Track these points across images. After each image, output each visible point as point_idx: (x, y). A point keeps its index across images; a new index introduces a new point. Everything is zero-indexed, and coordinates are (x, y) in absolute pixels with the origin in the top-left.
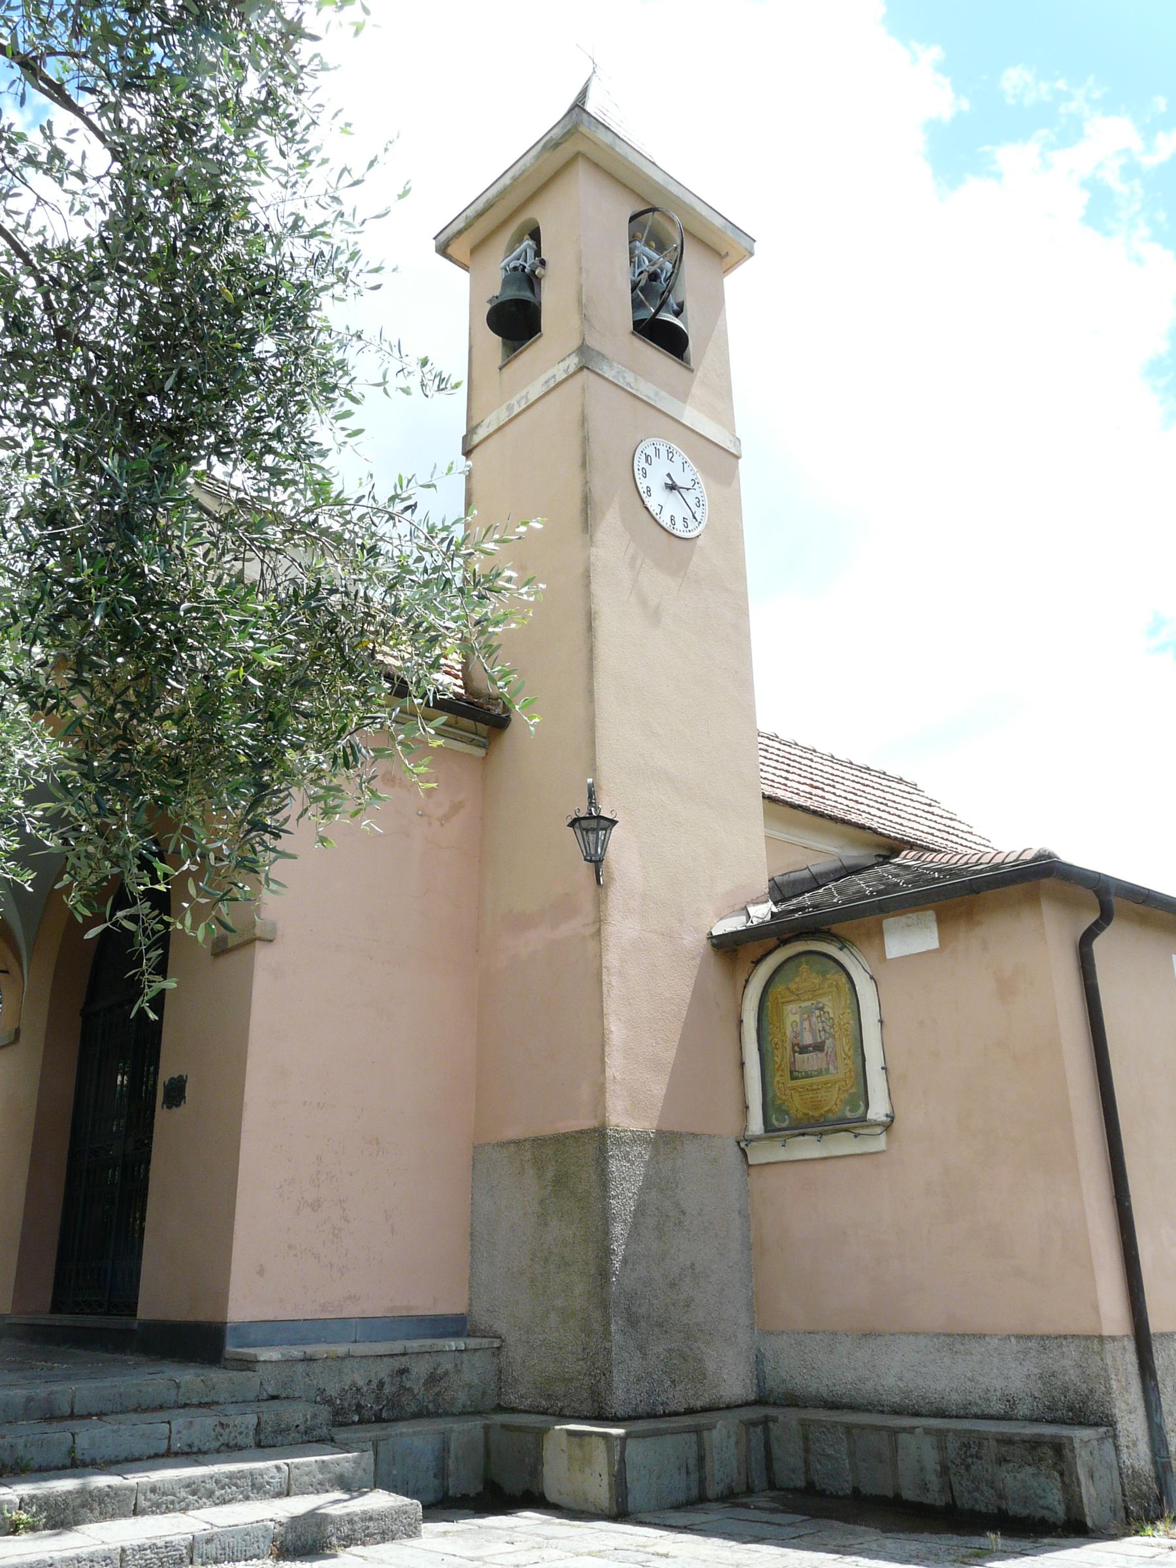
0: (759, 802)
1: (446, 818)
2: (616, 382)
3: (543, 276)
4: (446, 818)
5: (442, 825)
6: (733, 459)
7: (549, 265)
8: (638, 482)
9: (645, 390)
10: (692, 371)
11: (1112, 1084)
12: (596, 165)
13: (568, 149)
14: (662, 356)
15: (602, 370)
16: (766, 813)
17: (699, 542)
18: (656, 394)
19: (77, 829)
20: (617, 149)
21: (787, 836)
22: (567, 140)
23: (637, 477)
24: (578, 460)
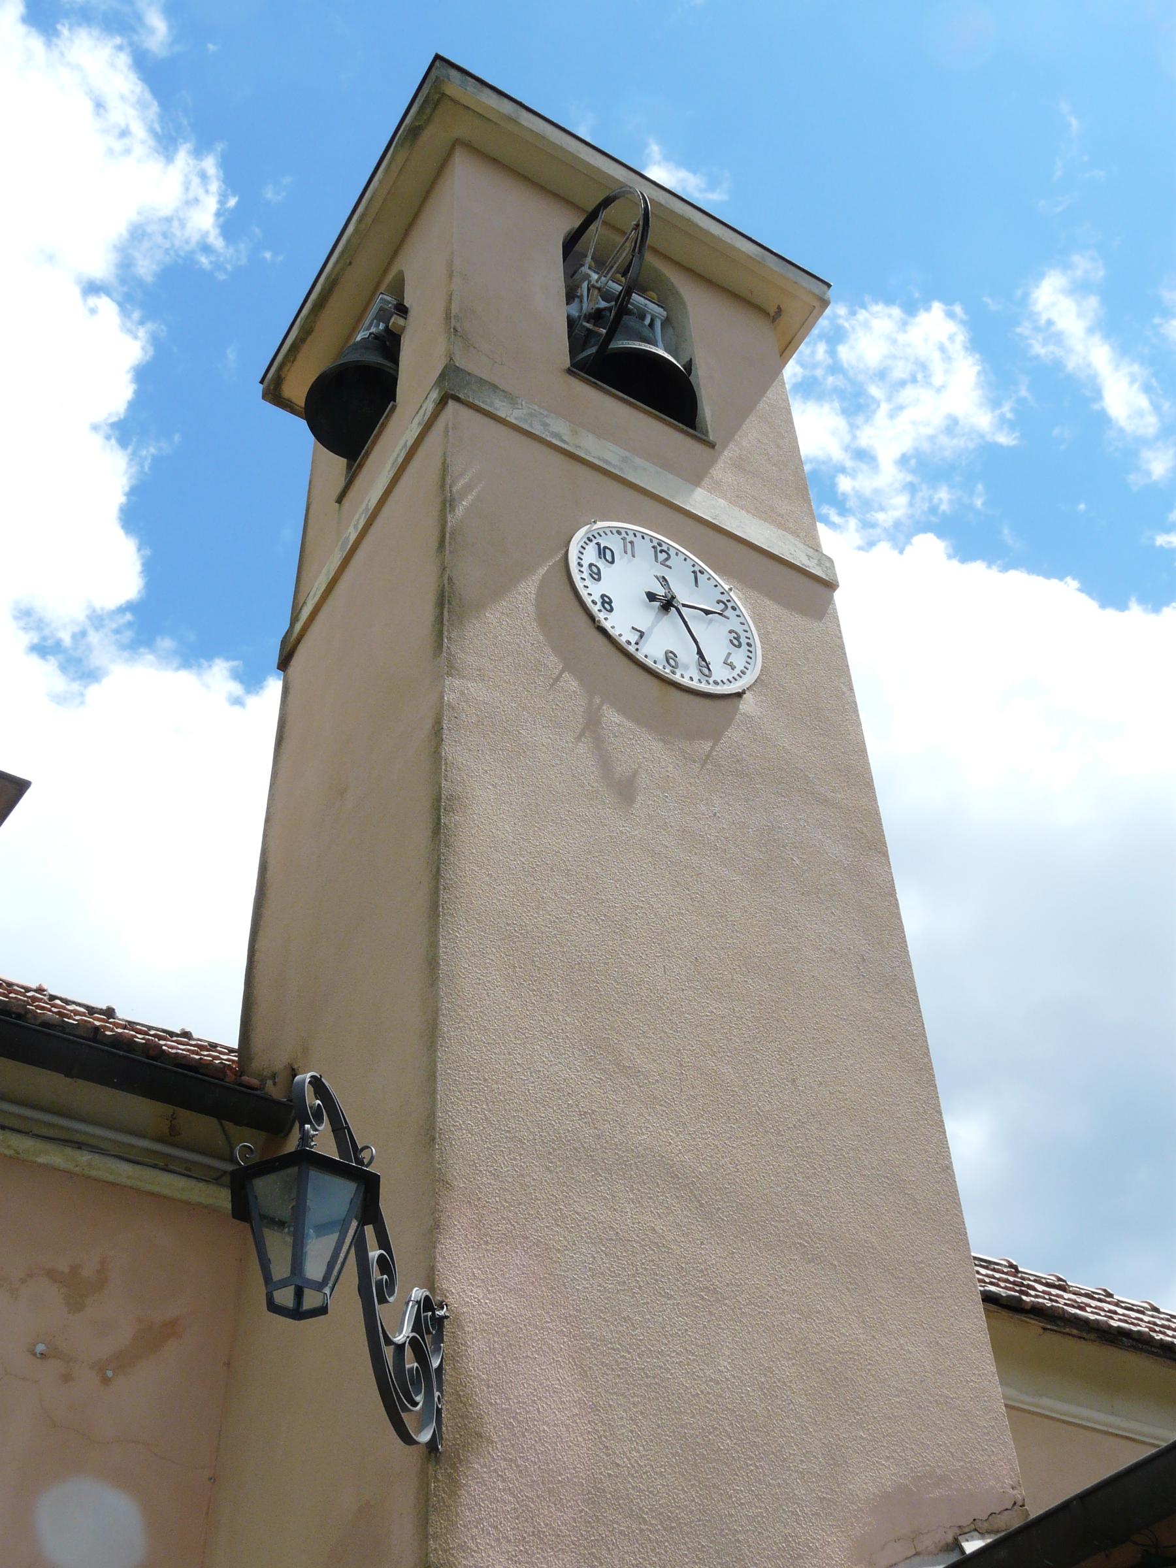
0: (975, 1319)
1: (122, 1361)
2: (526, 427)
3: (403, 328)
4: (122, 1361)
5: (106, 1381)
6: (819, 588)
7: (412, 314)
8: (583, 593)
9: (592, 448)
10: (712, 446)
11: (245, 980)
12: (494, 161)
13: (435, 136)
14: (641, 416)
15: (491, 404)
16: (1002, 1350)
17: (748, 705)
18: (624, 460)
19: (634, 1532)
20: (523, 123)
21: (1112, 1419)
22: (429, 120)
23: (579, 585)
24: (434, 543)
